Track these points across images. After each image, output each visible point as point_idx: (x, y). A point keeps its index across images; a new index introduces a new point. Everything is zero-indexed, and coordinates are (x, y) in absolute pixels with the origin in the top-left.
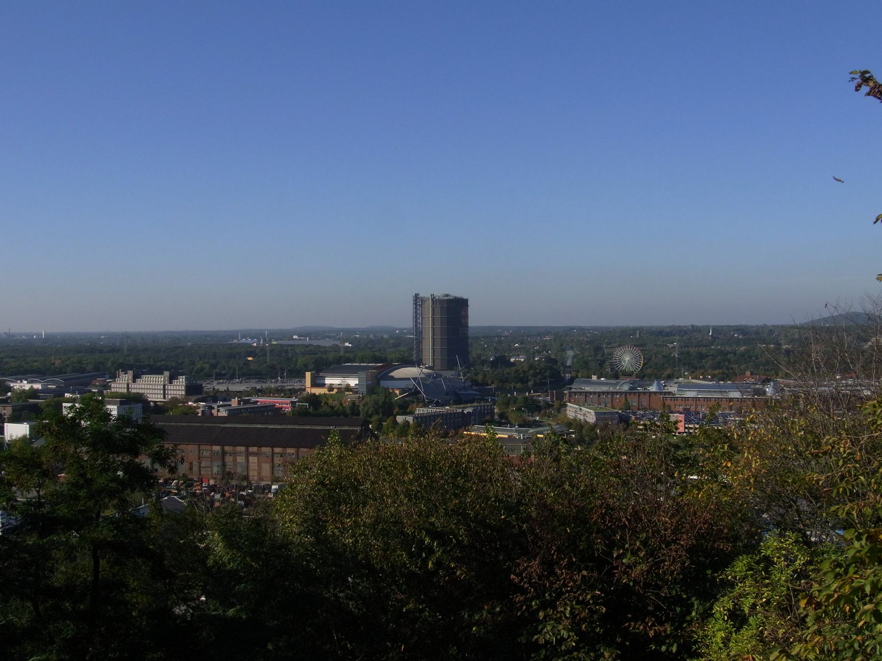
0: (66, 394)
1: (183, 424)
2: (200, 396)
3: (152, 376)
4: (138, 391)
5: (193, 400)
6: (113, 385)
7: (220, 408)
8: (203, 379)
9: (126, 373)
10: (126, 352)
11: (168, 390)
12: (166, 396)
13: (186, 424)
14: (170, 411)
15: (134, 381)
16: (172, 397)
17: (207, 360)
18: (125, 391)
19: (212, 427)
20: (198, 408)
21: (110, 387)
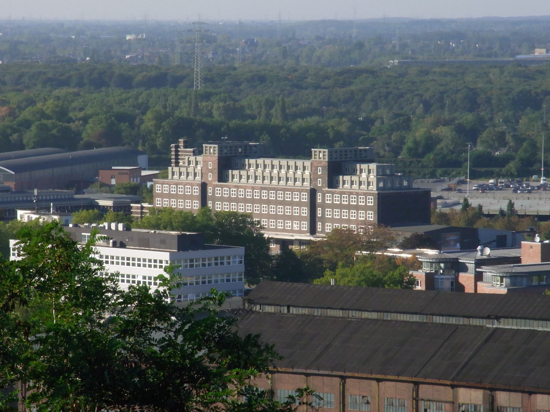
0: (20, 213)
1: (366, 315)
2: (422, 229)
3: (276, 162)
4: (233, 207)
5: (400, 240)
6: (158, 189)
7: (484, 269)
8: (433, 175)
9: (199, 152)
10: (199, 87)
11: (324, 206)
12: (319, 226)
13: (374, 316)
14: (328, 272)
15: (222, 177)
16: (336, 231)
17: (446, 115)
18: (196, 205)
19: (456, 327)
20: (416, 265)
21: (150, 195)
